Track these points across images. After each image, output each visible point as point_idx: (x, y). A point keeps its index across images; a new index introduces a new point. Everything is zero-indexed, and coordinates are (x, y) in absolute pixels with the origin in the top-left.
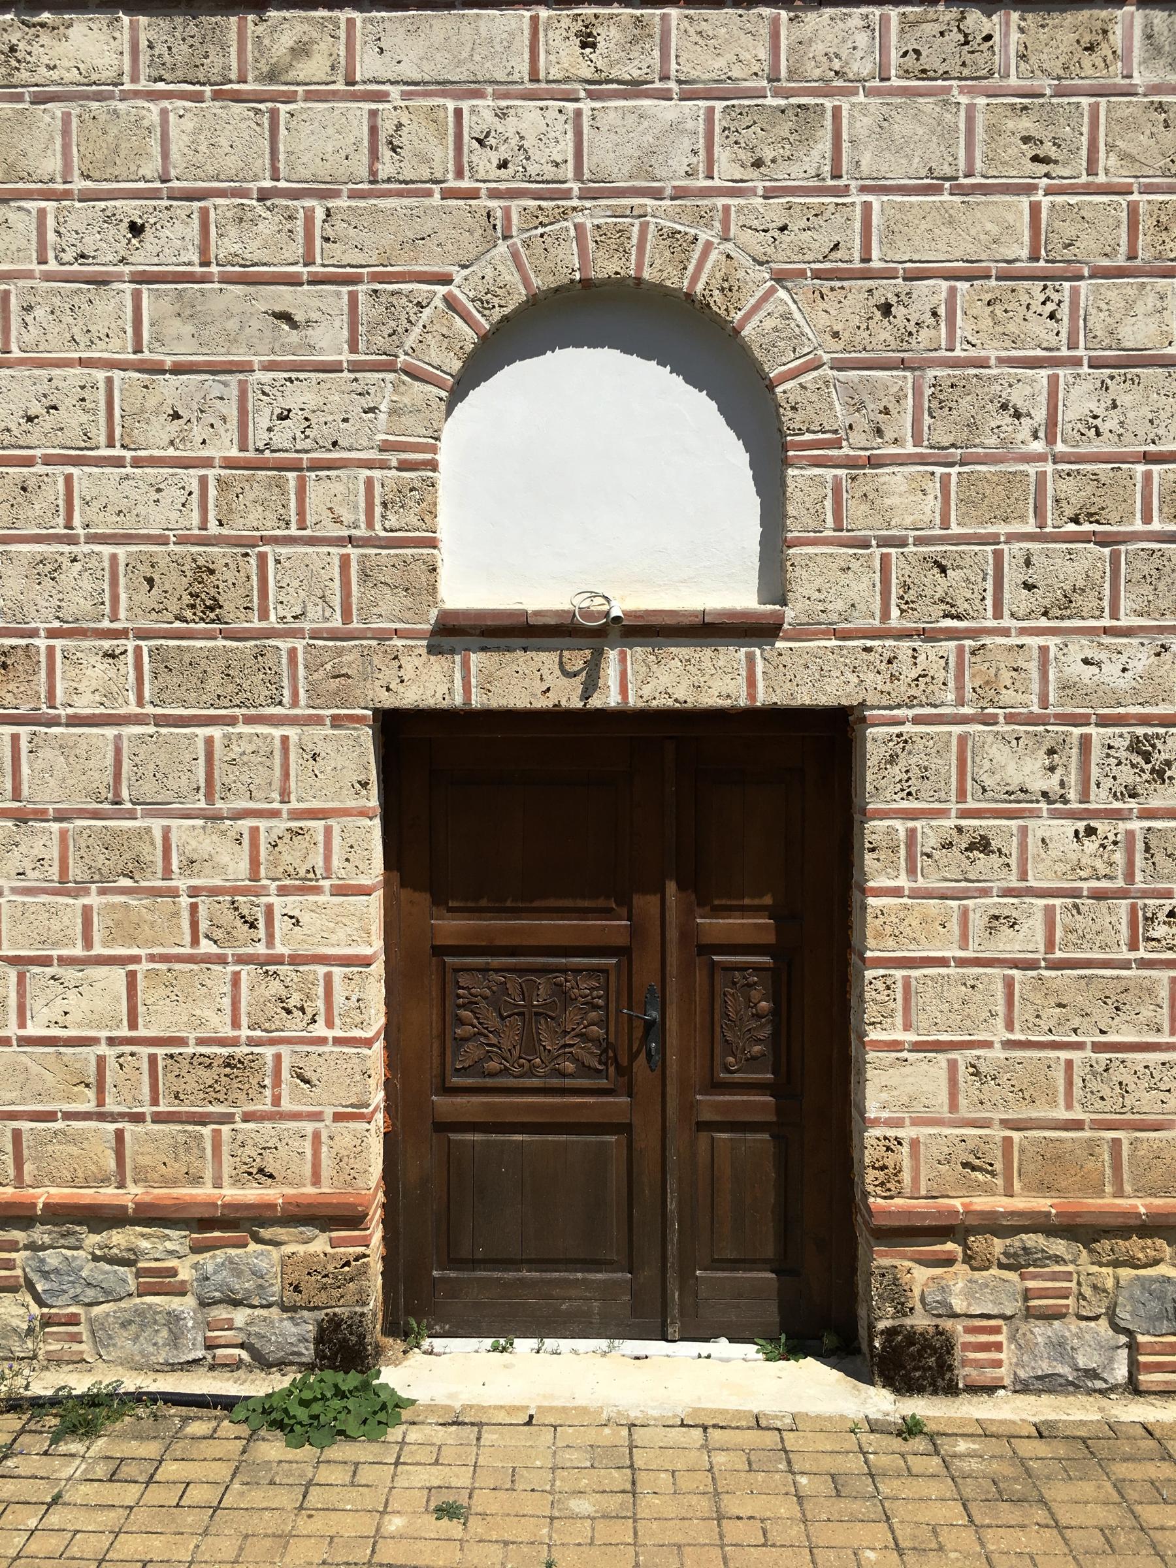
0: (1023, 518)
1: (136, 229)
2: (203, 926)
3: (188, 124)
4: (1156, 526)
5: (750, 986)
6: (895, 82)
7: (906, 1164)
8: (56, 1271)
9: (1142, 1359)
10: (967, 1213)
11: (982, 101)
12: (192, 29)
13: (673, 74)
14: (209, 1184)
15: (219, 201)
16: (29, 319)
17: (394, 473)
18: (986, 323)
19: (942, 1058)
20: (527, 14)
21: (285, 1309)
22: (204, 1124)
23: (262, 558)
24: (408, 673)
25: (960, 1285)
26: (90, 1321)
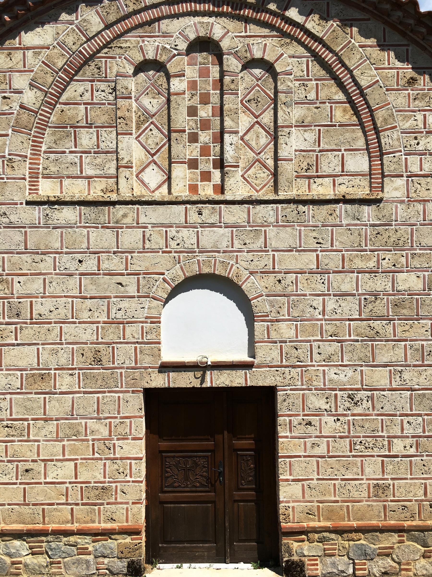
0: (317, 335)
1: (80, 261)
2: (96, 449)
3: (95, 234)
4: (352, 338)
5: (248, 460)
6: (280, 223)
7: (291, 513)
8: (54, 548)
9: (356, 567)
10: (307, 527)
11: (303, 228)
12: (96, 210)
13: (222, 222)
14: (97, 523)
15: (103, 254)
16: (51, 285)
17: (149, 324)
18: (306, 285)
19: (300, 483)
20: (184, 206)
21: (118, 558)
22: (96, 506)
23: (113, 348)
24: (153, 378)
25: (306, 547)
26: (64, 562)
